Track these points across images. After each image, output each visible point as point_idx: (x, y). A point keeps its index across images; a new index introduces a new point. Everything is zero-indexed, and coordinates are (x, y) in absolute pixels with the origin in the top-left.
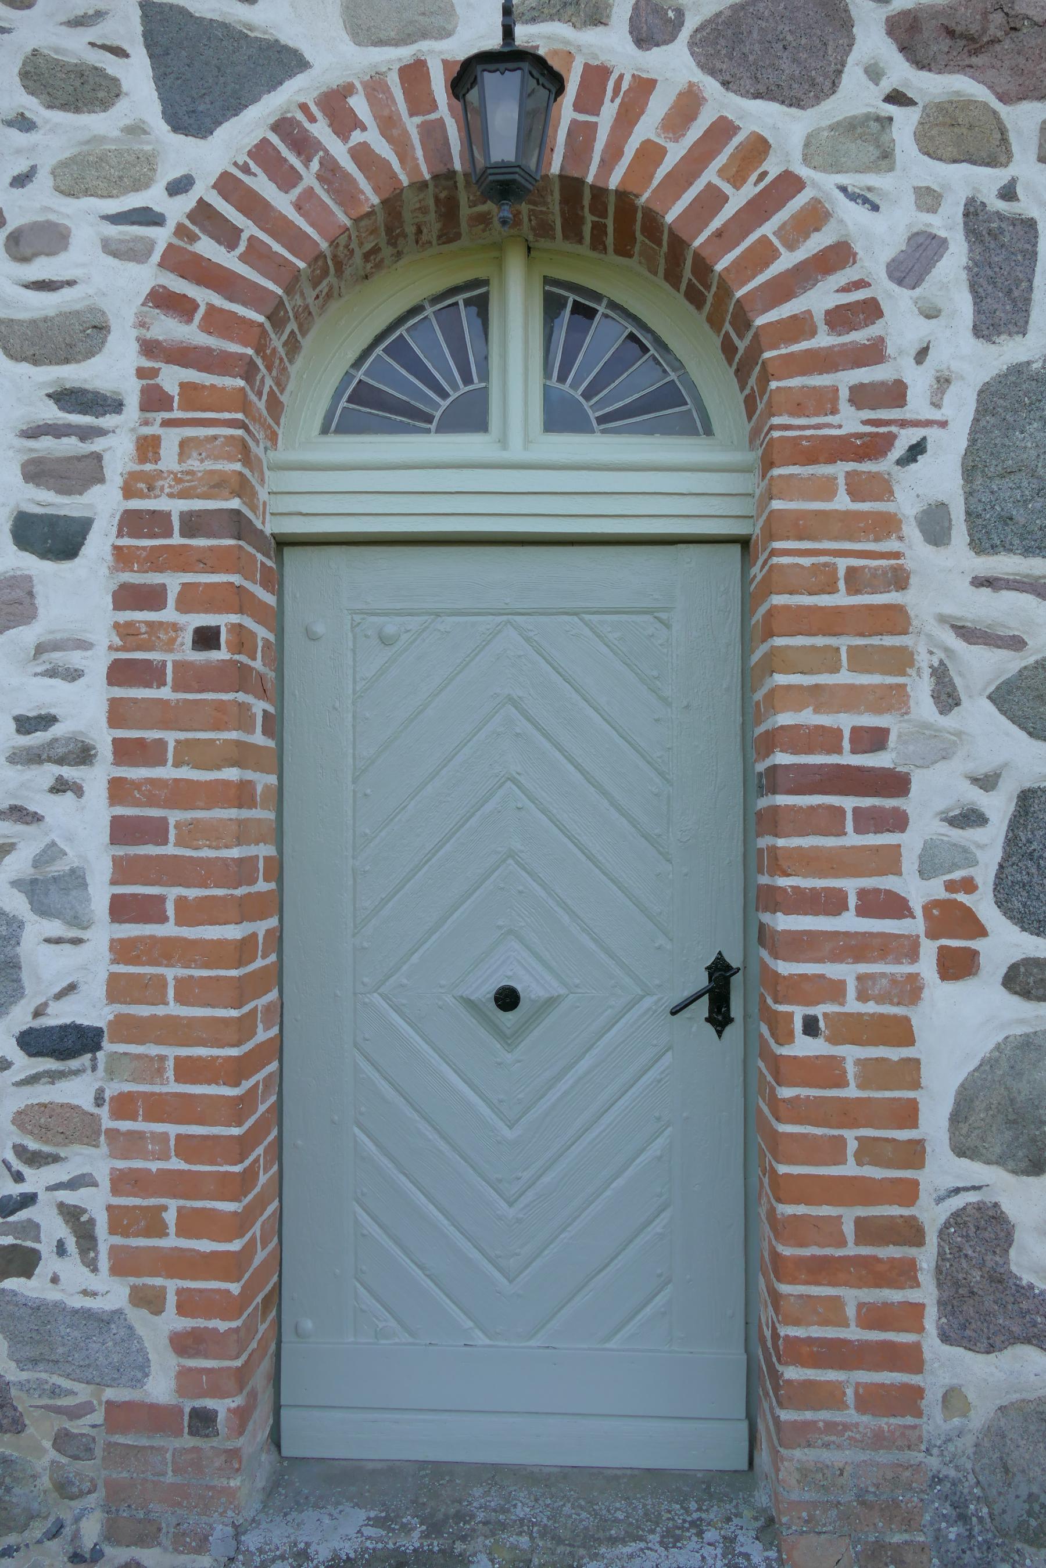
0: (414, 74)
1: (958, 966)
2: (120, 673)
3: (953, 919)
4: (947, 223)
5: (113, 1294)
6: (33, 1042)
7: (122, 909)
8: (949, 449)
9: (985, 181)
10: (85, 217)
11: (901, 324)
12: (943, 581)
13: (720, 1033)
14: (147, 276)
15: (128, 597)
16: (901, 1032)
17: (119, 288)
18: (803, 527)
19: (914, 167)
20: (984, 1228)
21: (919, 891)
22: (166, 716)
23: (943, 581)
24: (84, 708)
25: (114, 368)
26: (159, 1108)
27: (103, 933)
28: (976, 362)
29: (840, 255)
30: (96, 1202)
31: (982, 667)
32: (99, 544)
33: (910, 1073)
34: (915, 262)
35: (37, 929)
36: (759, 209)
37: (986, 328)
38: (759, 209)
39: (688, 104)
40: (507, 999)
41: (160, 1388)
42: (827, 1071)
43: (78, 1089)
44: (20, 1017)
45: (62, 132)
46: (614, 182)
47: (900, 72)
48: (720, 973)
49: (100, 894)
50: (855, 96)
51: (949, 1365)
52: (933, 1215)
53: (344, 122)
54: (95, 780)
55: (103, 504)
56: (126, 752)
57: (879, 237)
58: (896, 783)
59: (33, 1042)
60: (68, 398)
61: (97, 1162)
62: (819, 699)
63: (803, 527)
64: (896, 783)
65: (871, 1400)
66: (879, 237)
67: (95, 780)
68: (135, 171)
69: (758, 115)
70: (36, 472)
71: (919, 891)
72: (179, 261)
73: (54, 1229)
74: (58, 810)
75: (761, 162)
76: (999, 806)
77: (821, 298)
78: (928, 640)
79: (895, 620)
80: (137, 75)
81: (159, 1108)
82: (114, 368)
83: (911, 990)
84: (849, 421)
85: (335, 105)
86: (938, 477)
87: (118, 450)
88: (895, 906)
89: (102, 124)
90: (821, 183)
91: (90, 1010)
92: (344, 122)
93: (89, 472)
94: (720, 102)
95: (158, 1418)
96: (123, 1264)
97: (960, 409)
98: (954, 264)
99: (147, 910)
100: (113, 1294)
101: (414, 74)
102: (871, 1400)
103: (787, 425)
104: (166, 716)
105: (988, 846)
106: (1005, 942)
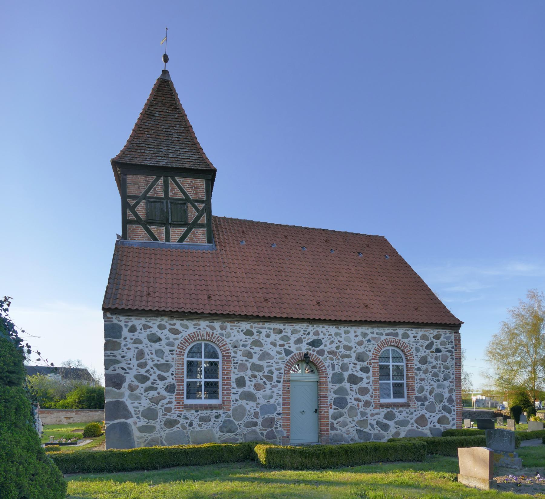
0: (300, 353)
1: (331, 408)
2: (283, 390)
3: (331, 405)
4: (330, 364)
5: (283, 430)
6: (277, 414)
7: (283, 405)
8: (330, 377)
9: (332, 362)
10: (280, 361)
11: (328, 370)
12: (330, 385)
13: (463, 323)
14: (284, 365)
15: (283, 386)
16: (328, 412)
17: (283, 366)
18: (323, 382)
19: (329, 361)
20: (333, 423)
21: (329, 404)
22: (286, 393)
23: (330, 385)
24: (281, 393)
25: (282, 371)
26: (285, 418)
27: (282, 407)
28: (332, 372)
29: (324, 366)
30: (281, 424)
31: (332, 390)
32: (282, 382)
33: (328, 414)
34: (328, 366)
35: (278, 407)
36: (320, 363)
37: (332, 370)
38: (320, 363)
39: (316, 356)
40: (303, 411)
41: (285, 435)
42: (324, 414)
43: (280, 417)
44: (276, 412)
45: (279, 356)
46: (322, 384)
47: (328, 355)
48: (316, 410)
49: (282, 404)
50: (325, 356)
51: (331, 432)
52: (330, 423)
53: (296, 356)
54: (281, 397)
55: (282, 380)
56: (283, 395)
57: (326, 365)
58: (327, 397)
59: (277, 414)
60: (280, 373)
61: (282, 421)
62: (323, 392)
63: (323, 382)
64: (327, 397)
65: (327, 434)
66: (326, 365)
67: (281, 397)
68: (283, 359)
69: (320, 357)
70: (278, 378)
71: (329, 404)
72: (286, 365)
73: (279, 426)
74: (279, 399)
75: (335, 413)
76: (333, 399)
77: (323, 368)
78: (329, 389)
79: (327, 388)
80: (283, 352)
81: (285, 418)
82: (282, 371)
83: (328, 410)
84: (325, 376)
85: (295, 355)
86: (330, 379)
87: (282, 376)
88: (327, 404)
89: (281, 356)
90: (323, 361)
91: (281, 412)
92: (296, 356)
93: (281, 378)
94: (318, 356)
95: (285, 437)
96: (283, 428)
97: (331, 375)
98: (331, 367)
99: (285, 405)
100: (283, 430)
101: (300, 353)
102: (327, 434)
103: (322, 376)
104: (286, 393)
105: (333, 401)
106: (334, 407)
